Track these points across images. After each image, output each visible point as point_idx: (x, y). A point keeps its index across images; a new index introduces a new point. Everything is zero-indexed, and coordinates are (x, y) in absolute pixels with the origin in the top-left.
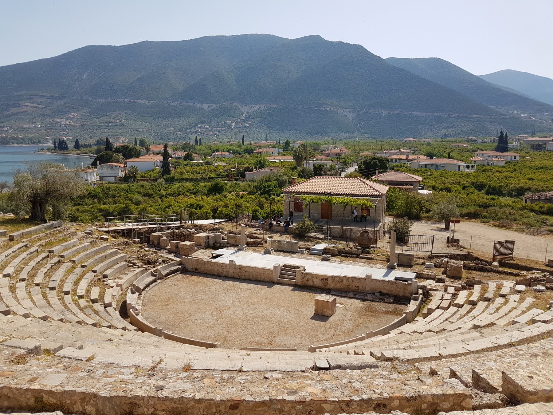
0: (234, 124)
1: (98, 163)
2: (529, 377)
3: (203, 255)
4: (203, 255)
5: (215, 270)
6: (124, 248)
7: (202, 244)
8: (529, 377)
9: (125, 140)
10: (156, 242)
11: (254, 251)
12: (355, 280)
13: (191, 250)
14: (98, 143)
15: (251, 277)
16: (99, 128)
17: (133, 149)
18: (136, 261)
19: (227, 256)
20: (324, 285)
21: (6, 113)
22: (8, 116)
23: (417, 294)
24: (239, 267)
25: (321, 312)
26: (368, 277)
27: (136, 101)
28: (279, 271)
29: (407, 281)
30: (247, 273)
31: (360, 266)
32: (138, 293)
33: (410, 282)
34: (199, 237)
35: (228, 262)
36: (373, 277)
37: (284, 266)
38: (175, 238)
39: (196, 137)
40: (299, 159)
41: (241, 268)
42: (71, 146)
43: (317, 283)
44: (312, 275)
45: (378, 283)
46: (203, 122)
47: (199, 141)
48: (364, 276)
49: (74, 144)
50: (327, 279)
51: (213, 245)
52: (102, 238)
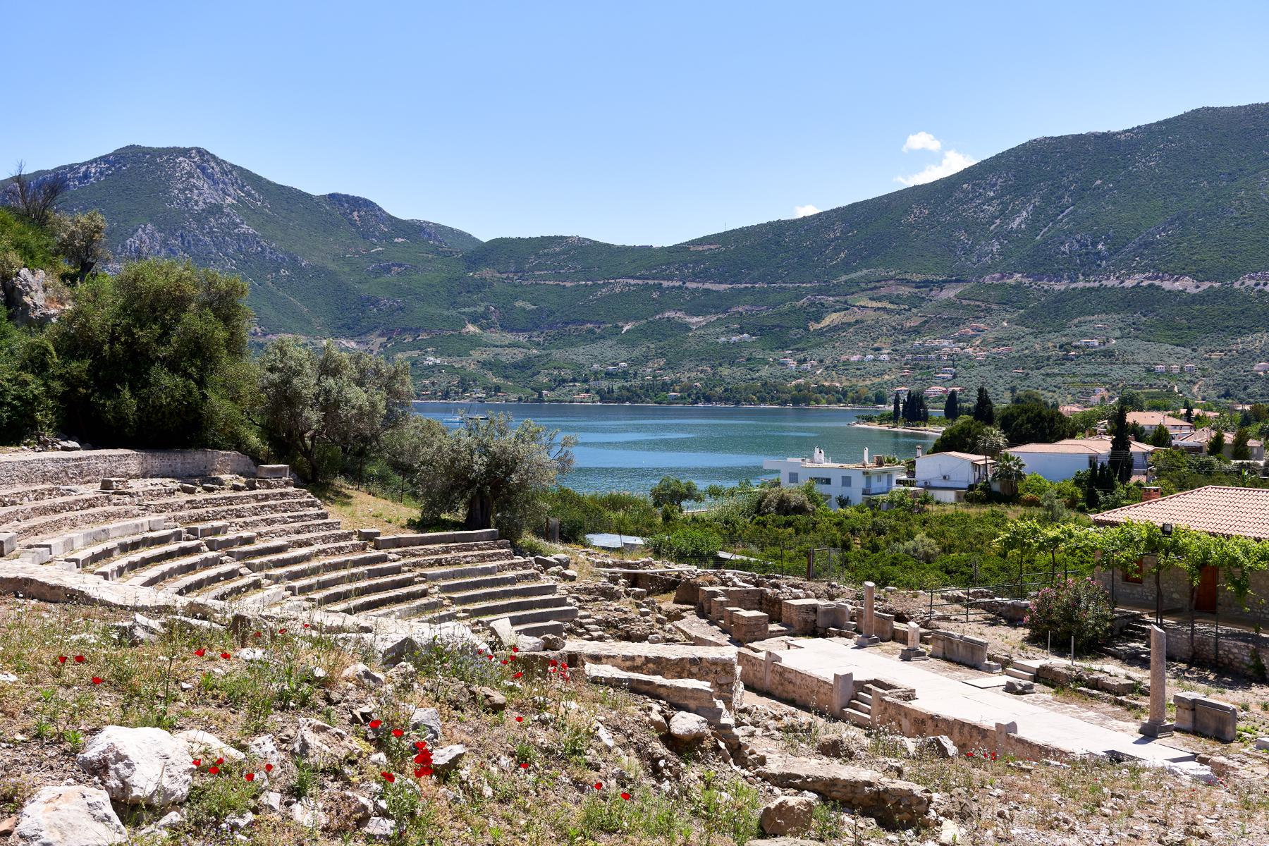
2: (145, 585)
6: (595, 600)
8: (145, 585)
9: (1112, 398)
15: (797, 697)
21: (814, 326)
22: (820, 333)
27: (1157, 283)
28: (851, 690)
36: (1022, 733)
37: (868, 682)
49: (943, 405)
50: (923, 722)
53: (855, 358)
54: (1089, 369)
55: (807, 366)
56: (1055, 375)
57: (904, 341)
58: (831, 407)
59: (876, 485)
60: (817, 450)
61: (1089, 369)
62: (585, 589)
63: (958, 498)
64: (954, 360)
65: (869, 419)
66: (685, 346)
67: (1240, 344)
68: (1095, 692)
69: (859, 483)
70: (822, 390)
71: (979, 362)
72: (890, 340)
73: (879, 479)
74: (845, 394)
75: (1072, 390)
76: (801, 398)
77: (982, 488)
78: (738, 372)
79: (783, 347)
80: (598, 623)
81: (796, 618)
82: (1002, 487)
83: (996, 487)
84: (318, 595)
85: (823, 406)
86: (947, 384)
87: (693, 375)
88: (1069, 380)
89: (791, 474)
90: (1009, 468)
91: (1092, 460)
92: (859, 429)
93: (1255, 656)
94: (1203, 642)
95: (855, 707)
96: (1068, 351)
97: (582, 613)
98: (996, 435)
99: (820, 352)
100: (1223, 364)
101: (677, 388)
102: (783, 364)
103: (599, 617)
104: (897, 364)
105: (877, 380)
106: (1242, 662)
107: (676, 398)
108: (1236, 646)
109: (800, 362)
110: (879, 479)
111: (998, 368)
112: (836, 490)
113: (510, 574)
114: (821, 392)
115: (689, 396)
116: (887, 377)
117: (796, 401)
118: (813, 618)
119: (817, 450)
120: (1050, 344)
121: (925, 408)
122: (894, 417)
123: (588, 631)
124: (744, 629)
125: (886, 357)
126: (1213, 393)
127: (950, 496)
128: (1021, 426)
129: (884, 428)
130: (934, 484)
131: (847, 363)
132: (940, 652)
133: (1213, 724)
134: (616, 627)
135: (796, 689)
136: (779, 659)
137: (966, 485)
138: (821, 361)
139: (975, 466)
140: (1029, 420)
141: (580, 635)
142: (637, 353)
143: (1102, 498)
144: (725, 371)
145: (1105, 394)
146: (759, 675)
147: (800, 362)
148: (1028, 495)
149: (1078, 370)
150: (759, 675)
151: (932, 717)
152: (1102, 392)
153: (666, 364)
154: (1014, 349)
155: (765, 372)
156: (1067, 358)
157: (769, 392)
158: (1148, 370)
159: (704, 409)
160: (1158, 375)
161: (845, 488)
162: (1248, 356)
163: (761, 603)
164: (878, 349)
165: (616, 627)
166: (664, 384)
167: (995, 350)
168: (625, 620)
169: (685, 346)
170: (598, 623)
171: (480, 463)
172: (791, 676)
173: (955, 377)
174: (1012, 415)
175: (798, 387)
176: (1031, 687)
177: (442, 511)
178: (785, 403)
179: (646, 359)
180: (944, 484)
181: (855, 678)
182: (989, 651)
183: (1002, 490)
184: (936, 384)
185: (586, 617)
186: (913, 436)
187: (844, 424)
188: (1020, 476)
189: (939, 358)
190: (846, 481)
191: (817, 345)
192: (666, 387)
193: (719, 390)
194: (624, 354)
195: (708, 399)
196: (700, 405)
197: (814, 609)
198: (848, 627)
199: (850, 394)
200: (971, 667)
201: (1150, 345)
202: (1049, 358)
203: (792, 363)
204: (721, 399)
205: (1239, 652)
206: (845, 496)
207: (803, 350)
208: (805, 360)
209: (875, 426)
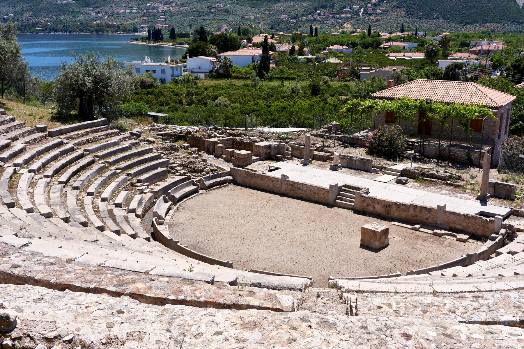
0: (362, 10)
1: (188, 57)
3: (260, 167)
4: (260, 167)
5: (266, 184)
6: (171, 153)
7: (261, 154)
9: (229, 29)
10: (211, 149)
11: (319, 166)
12: (424, 210)
13: (247, 161)
14: (197, 31)
16: (200, 14)
17: (232, 39)
18: (178, 168)
19: (292, 170)
20: (388, 212)
23: (497, 233)
24: (291, 183)
25: (368, 242)
26: (441, 209)
28: (336, 191)
29: (489, 217)
30: (300, 191)
31: (442, 194)
32: (171, 203)
33: (493, 219)
34: (259, 146)
35: (280, 177)
36: (448, 209)
37: (343, 186)
38: (235, 146)
39: (311, 26)
40: (432, 56)
41: (294, 184)
42: (166, 35)
43: (379, 208)
44: (374, 200)
45: (452, 217)
46: (324, 7)
47: (314, 30)
48: (435, 206)
50: (390, 206)
51: (273, 155)
52: (148, 141)
53: (121, 11)
54: (220, 17)
55: (100, 15)
56: (207, 20)
57: (142, 4)
58: (113, 34)
59: (176, 73)
60: (146, 57)
61: (220, 17)
62: (164, 148)
63: (206, 76)
64: (165, 12)
65: (137, 40)
66: (41, 5)
67: (276, 7)
68: (433, 180)
69: (169, 72)
70: (108, 26)
71: (175, 14)
72: (136, 3)
73: (177, 70)
74: (119, 28)
75: (214, 26)
76: (99, 29)
77: (215, 72)
78: (68, 18)
79: (88, 6)
80: (180, 166)
81: (262, 152)
82: (224, 71)
83: (221, 71)
84: (49, 172)
85: (110, 33)
86: (163, 23)
87: (47, 19)
88: (212, 22)
89: (162, 73)
90: (227, 63)
91: (253, 58)
92: (132, 44)
93: (468, 155)
94: (444, 150)
95: (341, 199)
96: (211, 9)
97: (171, 162)
98: (213, 48)
99: (105, 8)
100: (270, 15)
101: (40, 26)
102: (89, 14)
103: (179, 163)
104: (140, 14)
105: (132, 22)
106: (462, 157)
107: (40, 30)
108: (459, 151)
109: (97, 13)
110: (177, 70)
111: (183, 17)
112: (158, 75)
113: (126, 144)
114: (108, 27)
115: (46, 29)
116: (136, 20)
117: (97, 31)
118: (269, 151)
119: (146, 57)
120: (204, 6)
121: (162, 34)
122: (148, 39)
123: (177, 171)
124: (242, 160)
125: (135, 11)
126: (267, 27)
127: (202, 76)
128: (219, 43)
129: (144, 43)
130: (195, 70)
131: (118, 13)
132: (345, 164)
133: (504, 193)
134: (187, 167)
135: (303, 192)
136: (288, 177)
137: (208, 71)
138: (106, 13)
139: (212, 62)
140: (222, 41)
141: (174, 173)
142: (18, 9)
143: (266, 75)
144: (62, 18)
145: (227, 27)
146: (277, 186)
147: (97, 13)
148: (234, 74)
149: (215, 17)
150: (277, 186)
151: (396, 204)
152: (225, 27)
153: (32, 14)
154: (189, 8)
155: (81, 17)
156: (211, 12)
157: (84, 27)
158: (242, 18)
159: (54, 36)
160: (246, 20)
161: (163, 75)
162: (279, 12)
163: (233, 144)
164: (131, 7)
165: (187, 167)
166: (33, 23)
167: (181, 9)
168: (191, 163)
169: (41, 5)
170: (180, 166)
171: (89, 81)
172: (299, 186)
173: (166, 20)
174: (215, 38)
175: (97, 24)
176: (407, 180)
177: (71, 111)
178: (92, 32)
179: (22, 12)
180: (199, 70)
181: (339, 185)
182: (373, 163)
183: (224, 72)
184: (158, 23)
185: (174, 163)
186: (157, 47)
187: (125, 42)
188: (231, 66)
189: (158, 12)
190: (163, 71)
191: (104, 5)
192: (34, 25)
193: (61, 26)
194: (11, 10)
195: (56, 31)
196: (52, 33)
197: (269, 147)
198: (288, 154)
199: (121, 28)
200: (366, 171)
201: (242, 7)
202: (203, 12)
203: (93, 14)
204: (62, 31)
205: (461, 153)
206: (163, 78)
207: (98, 7)
208: (99, 12)
209: (140, 43)
